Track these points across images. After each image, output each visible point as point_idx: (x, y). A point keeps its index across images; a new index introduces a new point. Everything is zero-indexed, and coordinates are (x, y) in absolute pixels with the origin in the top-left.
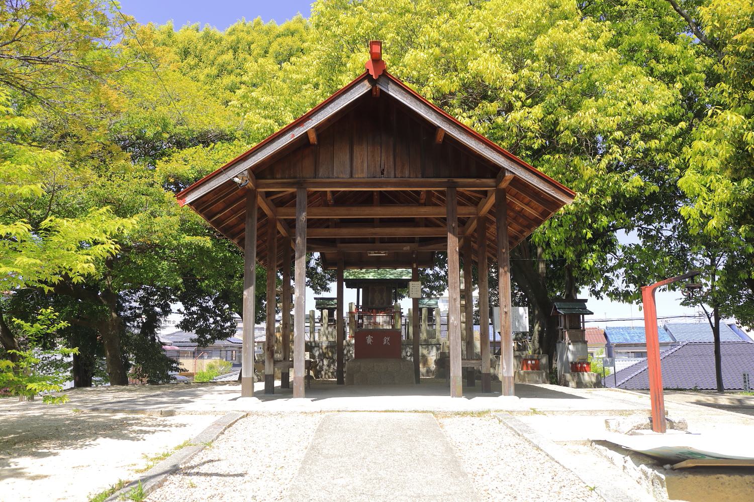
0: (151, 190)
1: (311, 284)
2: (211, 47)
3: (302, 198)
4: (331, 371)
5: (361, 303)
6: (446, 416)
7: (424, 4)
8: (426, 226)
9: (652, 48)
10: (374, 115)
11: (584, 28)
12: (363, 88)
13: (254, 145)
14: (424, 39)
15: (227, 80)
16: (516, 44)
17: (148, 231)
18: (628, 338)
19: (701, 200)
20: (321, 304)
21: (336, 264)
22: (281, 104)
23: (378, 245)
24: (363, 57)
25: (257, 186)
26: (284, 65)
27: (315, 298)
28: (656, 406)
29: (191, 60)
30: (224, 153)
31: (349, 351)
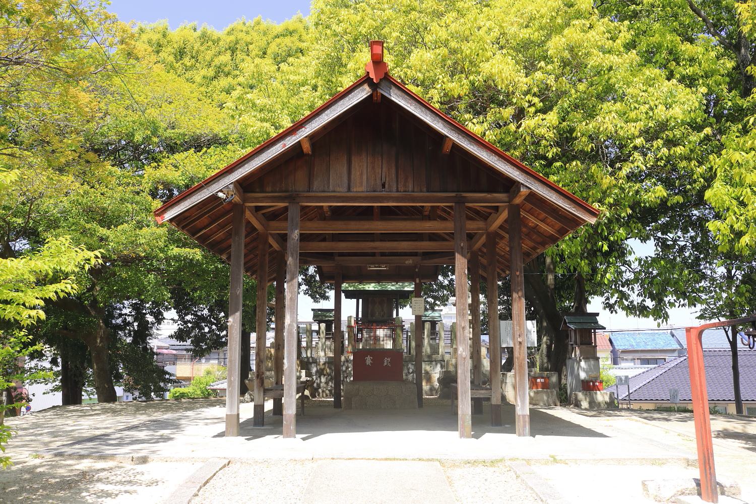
0: (138, 198)
1: (310, 292)
2: (209, 48)
3: (294, 213)
4: (329, 389)
5: (360, 316)
6: (454, 466)
7: (430, 3)
9: (672, 49)
10: (376, 124)
11: (603, 29)
12: (363, 93)
13: (249, 150)
14: (431, 38)
15: (224, 82)
16: (525, 46)
17: (132, 243)
18: (634, 344)
19: (732, 214)
20: (319, 316)
21: (333, 274)
22: (278, 106)
23: (379, 258)
24: (364, 57)
25: (245, 200)
26: (282, 65)
27: (312, 310)
28: (706, 475)
29: (187, 61)
30: (217, 159)
31: (347, 368)
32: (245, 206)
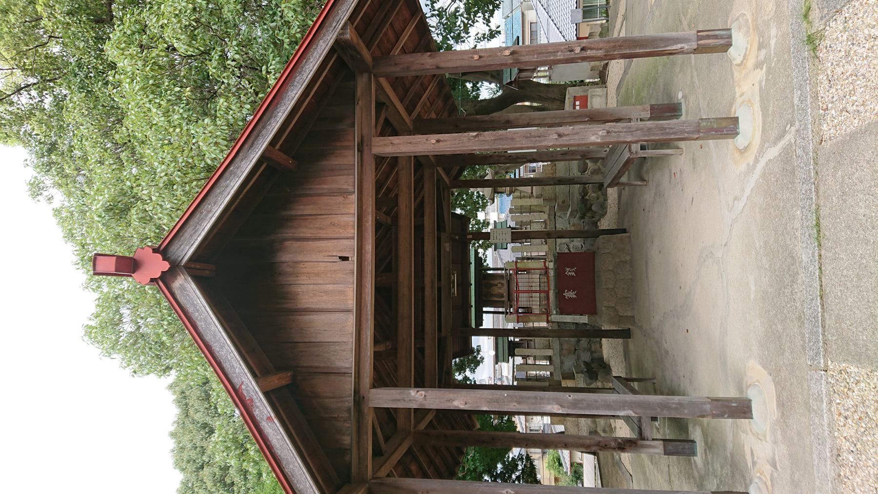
8: (423, 216)
12: (188, 289)
32: (374, 478)
